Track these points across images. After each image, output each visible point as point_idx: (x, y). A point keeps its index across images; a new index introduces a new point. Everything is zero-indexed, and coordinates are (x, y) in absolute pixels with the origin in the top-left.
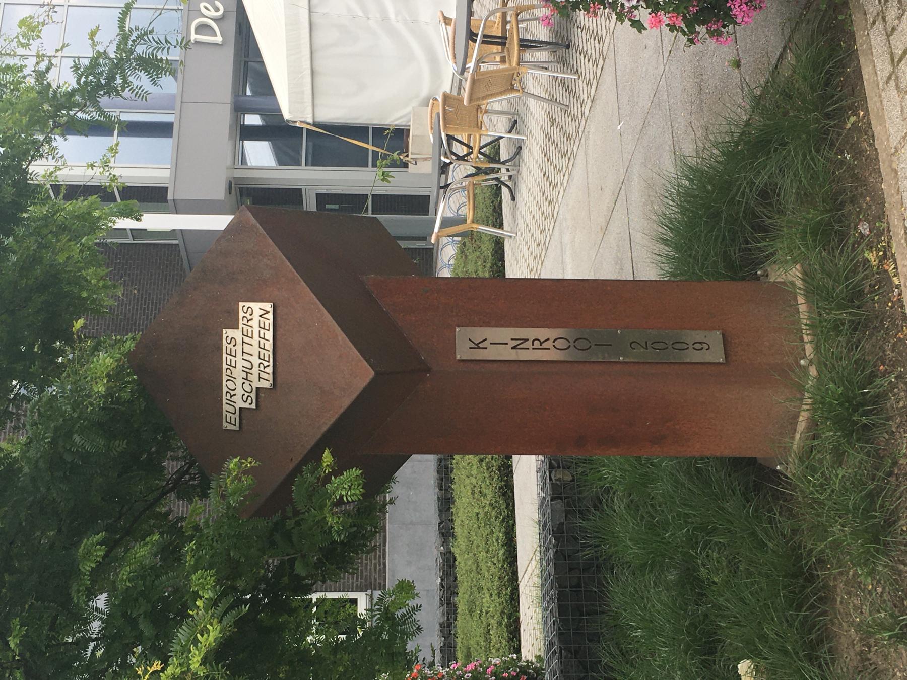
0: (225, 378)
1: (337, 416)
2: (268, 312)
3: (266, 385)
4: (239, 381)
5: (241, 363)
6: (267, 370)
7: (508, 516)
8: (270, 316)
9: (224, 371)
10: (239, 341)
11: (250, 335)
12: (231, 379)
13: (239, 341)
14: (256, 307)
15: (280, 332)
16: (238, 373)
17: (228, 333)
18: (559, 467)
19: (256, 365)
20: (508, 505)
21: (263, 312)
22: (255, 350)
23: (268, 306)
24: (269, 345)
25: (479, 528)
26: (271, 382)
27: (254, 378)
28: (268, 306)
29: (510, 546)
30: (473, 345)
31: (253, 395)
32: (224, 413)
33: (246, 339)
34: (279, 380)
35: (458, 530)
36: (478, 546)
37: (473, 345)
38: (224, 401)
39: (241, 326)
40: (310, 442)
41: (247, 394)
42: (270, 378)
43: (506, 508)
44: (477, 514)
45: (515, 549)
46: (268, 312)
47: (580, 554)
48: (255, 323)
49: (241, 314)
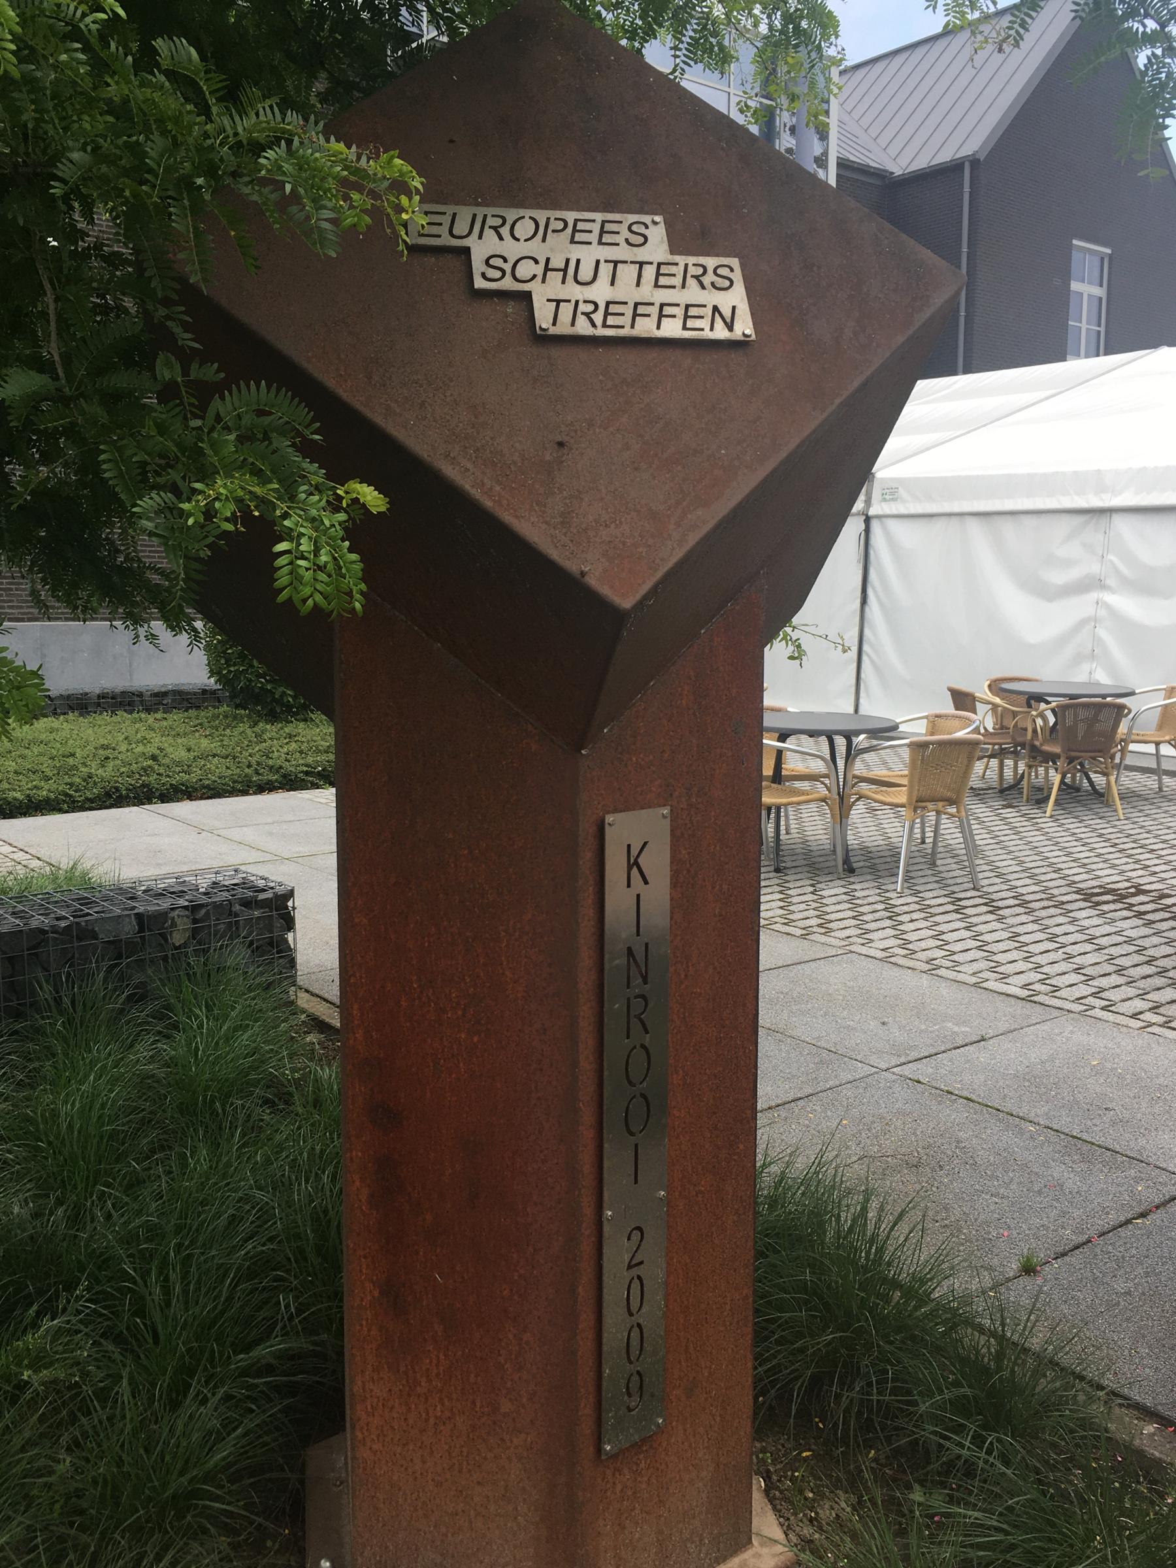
0: (541, 216)
1: (488, 504)
2: (730, 328)
3: (543, 316)
5: (588, 255)
6: (582, 321)
7: (74, 802)
9: (559, 214)
10: (642, 254)
11: (663, 281)
12: (542, 231)
13: (642, 254)
14: (736, 298)
15: (686, 359)
16: (558, 249)
17: (657, 234)
18: (195, 921)
19: (592, 293)
20: (91, 801)
21: (727, 313)
22: (626, 290)
23: (744, 327)
24: (646, 327)
25: (52, 758)
26: (553, 331)
27: (554, 287)
28: (744, 327)
29: (28, 807)
30: (634, 852)
31: (507, 284)
32: (450, 209)
33: (649, 272)
34: (556, 352)
35: (42, 724)
36: (23, 757)
37: (634, 852)
38: (480, 211)
39: (681, 260)
40: (421, 438)
41: (508, 267)
42: (563, 328)
43: (87, 799)
44: (73, 755)
45: (25, 814)
46: (730, 328)
47: (41, 975)
48: (693, 294)
49: (711, 262)
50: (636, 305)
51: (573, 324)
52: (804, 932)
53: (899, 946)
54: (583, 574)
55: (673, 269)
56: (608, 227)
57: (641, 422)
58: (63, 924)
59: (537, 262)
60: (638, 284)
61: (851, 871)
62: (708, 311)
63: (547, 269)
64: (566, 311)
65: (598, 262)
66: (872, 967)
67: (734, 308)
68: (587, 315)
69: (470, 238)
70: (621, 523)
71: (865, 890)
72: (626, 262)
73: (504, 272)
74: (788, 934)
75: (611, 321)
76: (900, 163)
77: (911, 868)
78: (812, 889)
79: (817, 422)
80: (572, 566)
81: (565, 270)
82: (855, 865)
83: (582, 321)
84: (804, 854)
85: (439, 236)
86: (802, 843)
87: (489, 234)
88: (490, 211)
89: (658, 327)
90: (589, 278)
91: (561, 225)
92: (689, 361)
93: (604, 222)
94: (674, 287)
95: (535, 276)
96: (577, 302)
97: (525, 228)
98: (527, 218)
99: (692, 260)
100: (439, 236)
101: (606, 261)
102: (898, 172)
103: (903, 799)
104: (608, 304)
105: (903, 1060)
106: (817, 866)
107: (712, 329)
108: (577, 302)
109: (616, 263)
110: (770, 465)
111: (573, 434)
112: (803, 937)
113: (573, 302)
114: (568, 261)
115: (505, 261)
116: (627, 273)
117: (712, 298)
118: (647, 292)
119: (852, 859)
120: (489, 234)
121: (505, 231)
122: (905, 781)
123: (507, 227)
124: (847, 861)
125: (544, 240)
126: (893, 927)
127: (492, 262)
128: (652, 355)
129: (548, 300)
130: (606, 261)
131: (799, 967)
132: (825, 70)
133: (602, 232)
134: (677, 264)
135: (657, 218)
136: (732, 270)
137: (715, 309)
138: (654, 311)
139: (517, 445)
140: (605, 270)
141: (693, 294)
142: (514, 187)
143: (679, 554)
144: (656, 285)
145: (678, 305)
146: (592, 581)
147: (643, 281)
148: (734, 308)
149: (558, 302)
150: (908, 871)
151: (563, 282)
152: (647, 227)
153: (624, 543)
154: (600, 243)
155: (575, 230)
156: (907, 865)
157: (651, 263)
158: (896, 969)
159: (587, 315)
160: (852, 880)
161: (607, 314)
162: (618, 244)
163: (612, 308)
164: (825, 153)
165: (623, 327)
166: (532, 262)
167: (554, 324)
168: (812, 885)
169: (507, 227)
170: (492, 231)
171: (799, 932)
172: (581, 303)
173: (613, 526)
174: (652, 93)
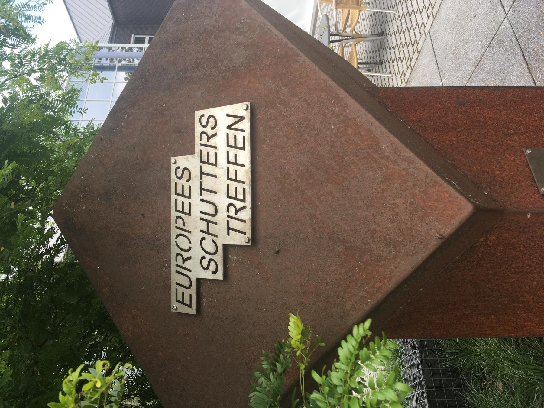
0: (174, 232)
4: (196, 236)
5: (198, 207)
6: (241, 215)
8: (246, 125)
10: (195, 173)
11: (212, 160)
12: (184, 233)
13: (195, 173)
14: (222, 114)
16: (194, 224)
17: (182, 161)
19: (222, 208)
22: (220, 184)
23: (241, 109)
24: (244, 174)
26: (249, 234)
27: (220, 229)
28: (241, 109)
31: (219, 258)
32: (174, 286)
33: (207, 168)
34: (262, 231)
38: (174, 268)
39: (198, 148)
41: (208, 257)
42: (247, 228)
48: (220, 141)
49: (199, 129)
50: (229, 179)
51: (244, 221)
52: (416, 52)
53: (427, 11)
54: (442, 237)
55: (204, 154)
56: (179, 191)
57: (311, 182)
58: (418, 353)
59: (203, 239)
60: (216, 176)
61: (383, 33)
62: (231, 132)
63: (208, 233)
64: (234, 224)
65: (202, 200)
66: (439, 23)
67: (228, 115)
68: (237, 211)
69: (191, 277)
70: (393, 204)
71: (393, 27)
72: (201, 183)
73: (211, 260)
74: (417, 59)
75: (240, 196)
76: (110, 21)
77: (383, 7)
78: (392, 49)
79: (307, 60)
80: (433, 244)
81: (209, 222)
82: (380, 31)
83: (241, 215)
84: (373, 52)
85: (191, 295)
86: (367, 53)
87: (187, 265)
88: (173, 263)
89: (244, 166)
90: (213, 207)
91: (180, 220)
92: (264, 146)
93: (177, 194)
94: (216, 154)
95: (213, 241)
96: (229, 217)
97: (183, 242)
98: (176, 240)
99: (197, 141)
100: (191, 295)
101: (201, 195)
102: (112, 21)
103: (357, 12)
104: (229, 197)
105: (500, 7)
106: (379, 48)
107: (243, 131)
108: (229, 217)
109: (202, 189)
110: (342, 93)
111: (322, 230)
112: (419, 53)
113: (229, 219)
114: (202, 219)
115: (203, 258)
116: (208, 182)
117: (222, 130)
118: (220, 170)
119: (377, 32)
120: (187, 265)
121: (186, 255)
122: (346, 11)
123: (183, 253)
124: (378, 35)
125: (190, 232)
126: (415, 14)
127: (205, 266)
128: (260, 169)
129: (228, 234)
130: (201, 195)
131: (437, 54)
132: (79, 48)
133: (182, 195)
134: (201, 151)
135: (173, 161)
136: (203, 116)
137: (229, 127)
138: (232, 168)
139: (332, 268)
140: (206, 196)
141: (220, 141)
142: (156, 245)
143: (420, 164)
144: (215, 165)
145: (228, 152)
146: (448, 231)
147: (213, 173)
148: (228, 115)
149: (229, 229)
150: (384, 8)
151: (216, 224)
152: (178, 168)
153: (412, 204)
154: (190, 197)
155: (182, 212)
156: (380, 8)
157: (201, 167)
158: (440, 12)
159: (237, 211)
160: (388, 33)
161: (235, 198)
162: (190, 187)
163: (232, 194)
164: (107, 47)
165: (244, 189)
166: (204, 242)
167: (244, 233)
168: (390, 49)
169: (183, 253)
170: (186, 262)
171: (416, 54)
172: (229, 214)
173: (396, 210)
174: (100, 156)
